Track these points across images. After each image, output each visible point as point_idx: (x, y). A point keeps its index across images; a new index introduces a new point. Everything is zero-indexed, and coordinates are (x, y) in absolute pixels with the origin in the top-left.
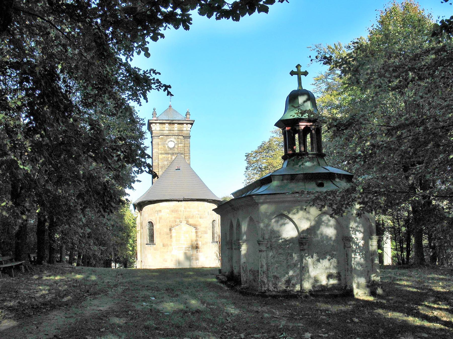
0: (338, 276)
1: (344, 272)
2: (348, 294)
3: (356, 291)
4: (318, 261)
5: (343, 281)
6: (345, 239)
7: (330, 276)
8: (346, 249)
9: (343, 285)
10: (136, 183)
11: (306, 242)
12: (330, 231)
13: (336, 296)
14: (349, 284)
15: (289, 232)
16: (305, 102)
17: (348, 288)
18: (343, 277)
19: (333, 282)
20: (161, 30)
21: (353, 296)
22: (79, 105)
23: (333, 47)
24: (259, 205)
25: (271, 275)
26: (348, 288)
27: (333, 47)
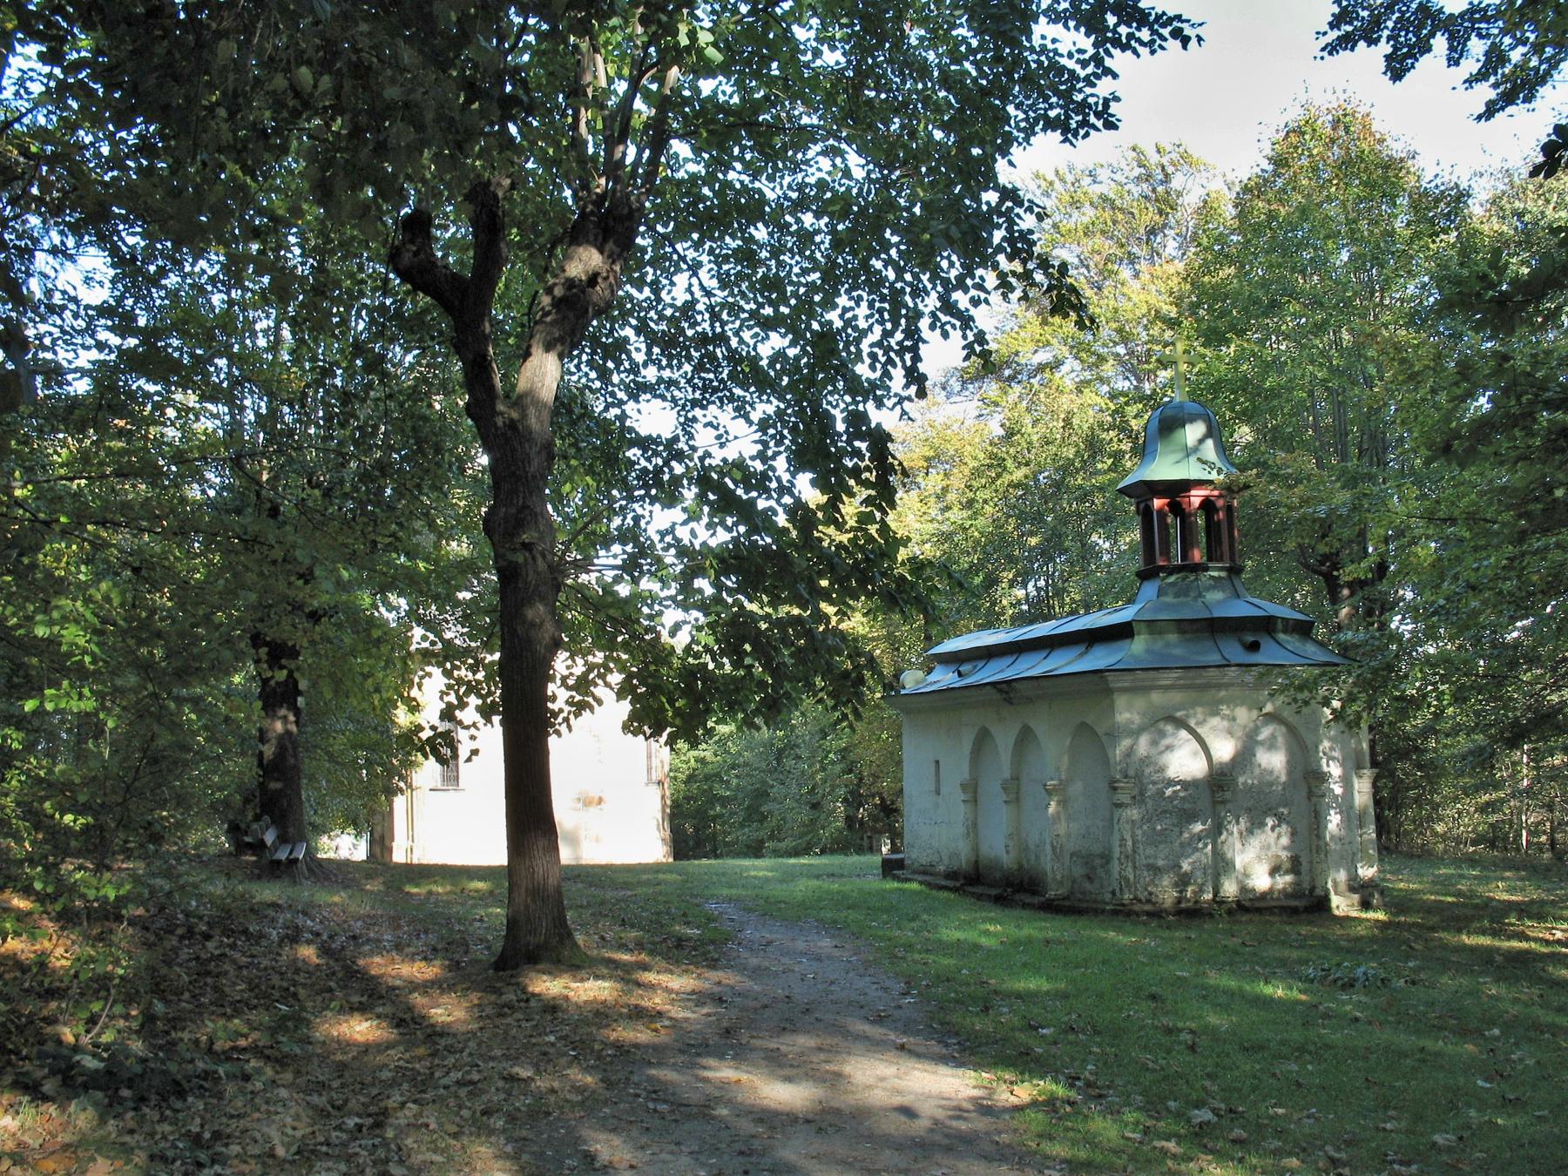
0: (1295, 866)
1: (1306, 857)
2: (1320, 905)
3: (1335, 900)
4: (1250, 832)
5: (1306, 878)
6: (1309, 778)
7: (1274, 871)
8: (1314, 799)
9: (1306, 886)
10: (1129, 53)
11: (1220, 791)
12: (1274, 761)
13: (1294, 911)
14: (1319, 884)
15: (1184, 762)
16: (1201, 441)
17: (1319, 892)
18: (1305, 866)
19: (1283, 881)
20: (550, 693)
21: (1329, 909)
22: (666, 549)
23: (1051, 176)
24: (1116, 696)
25: (1141, 860)
26: (1319, 892)
27: (1051, 176)
